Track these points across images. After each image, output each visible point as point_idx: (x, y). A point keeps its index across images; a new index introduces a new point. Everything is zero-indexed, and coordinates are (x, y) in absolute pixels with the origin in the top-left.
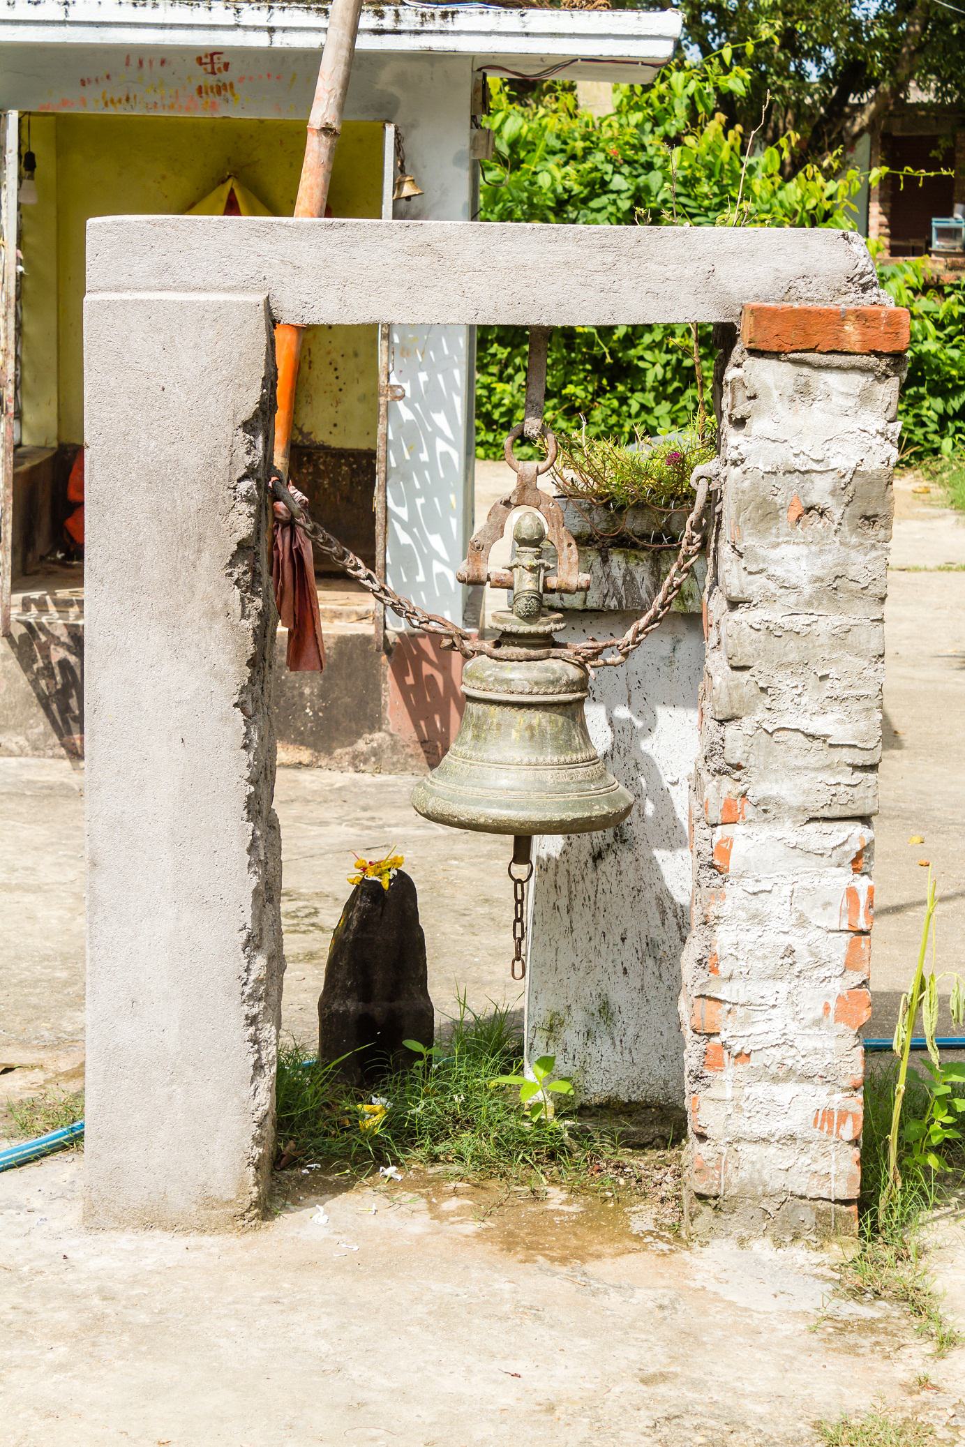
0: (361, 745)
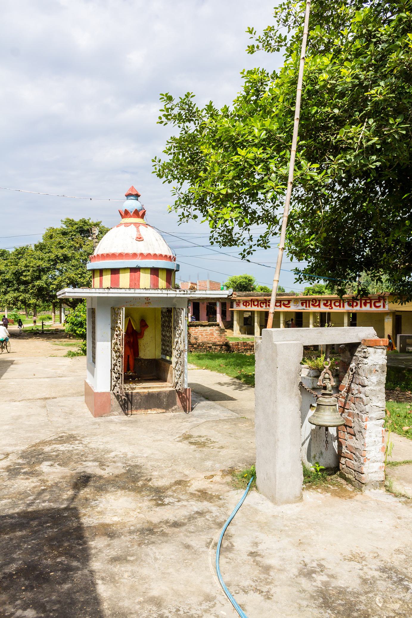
0: (173, 408)
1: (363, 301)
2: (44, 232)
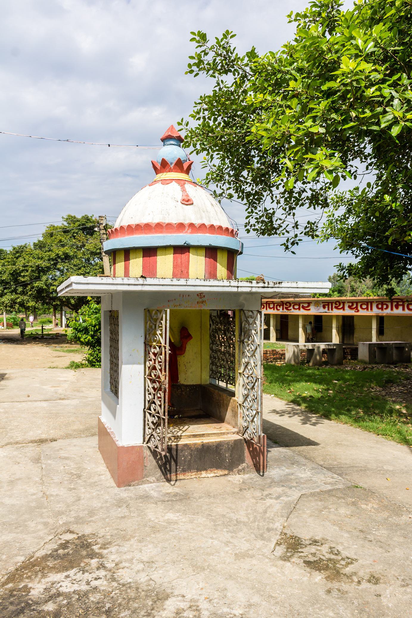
0: (240, 468)
1: (394, 304)
2: (44, 230)
